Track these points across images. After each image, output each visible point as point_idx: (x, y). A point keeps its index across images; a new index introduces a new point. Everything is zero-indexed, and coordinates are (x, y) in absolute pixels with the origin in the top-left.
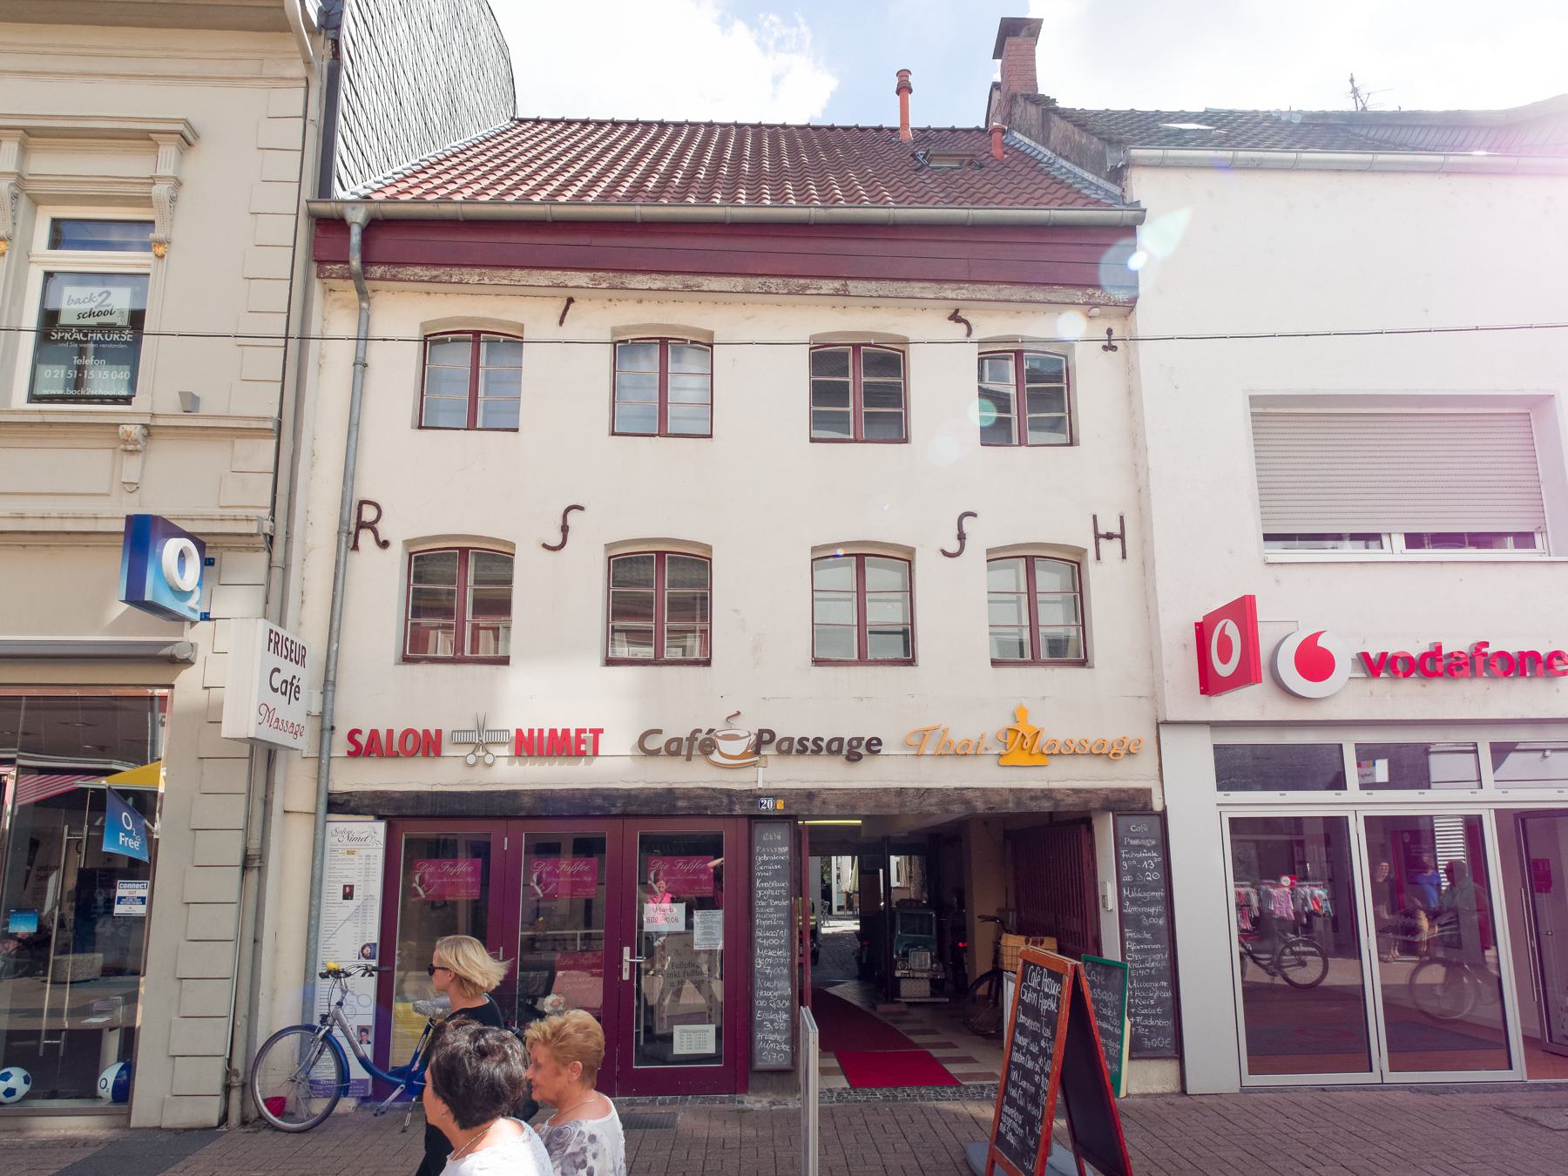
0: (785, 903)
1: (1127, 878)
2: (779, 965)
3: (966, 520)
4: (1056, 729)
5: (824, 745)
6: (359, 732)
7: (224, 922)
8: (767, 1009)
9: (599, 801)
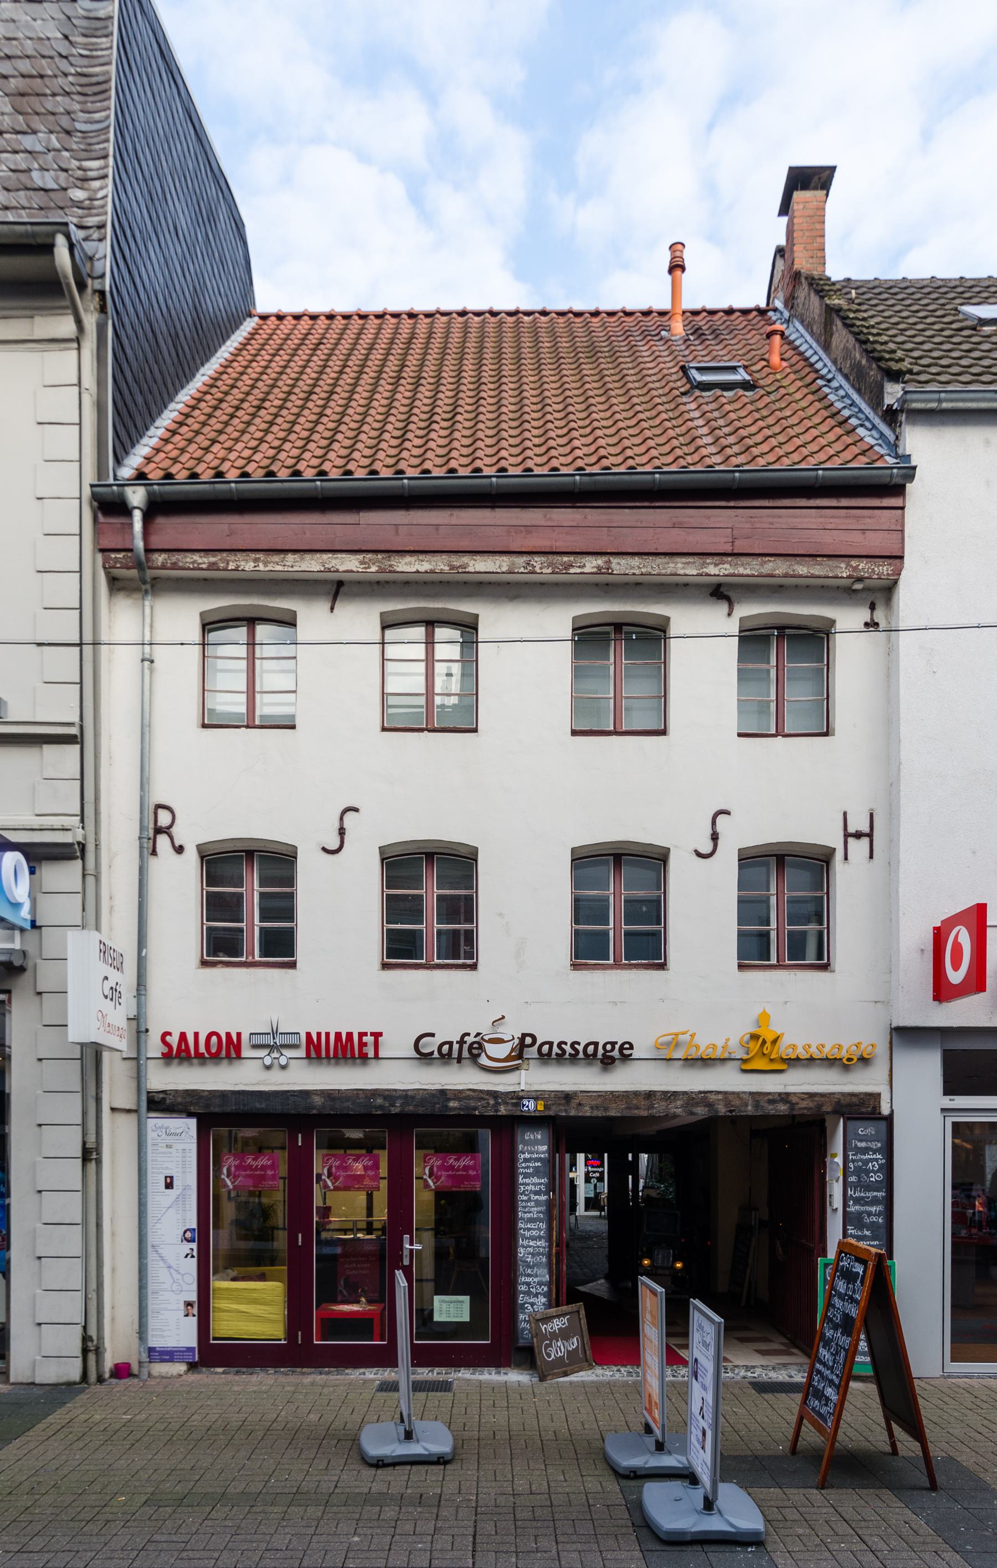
0: (543, 1198)
1: (853, 1179)
2: (539, 1254)
3: (720, 819)
4: (797, 1036)
5: (580, 1048)
6: (169, 1034)
7: (72, 1208)
8: (528, 1293)
9: (380, 1101)
